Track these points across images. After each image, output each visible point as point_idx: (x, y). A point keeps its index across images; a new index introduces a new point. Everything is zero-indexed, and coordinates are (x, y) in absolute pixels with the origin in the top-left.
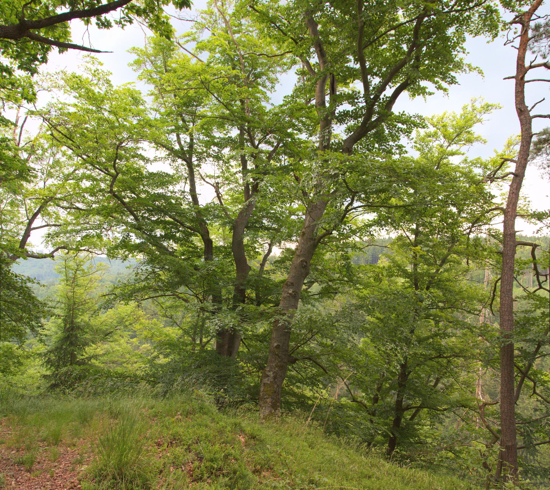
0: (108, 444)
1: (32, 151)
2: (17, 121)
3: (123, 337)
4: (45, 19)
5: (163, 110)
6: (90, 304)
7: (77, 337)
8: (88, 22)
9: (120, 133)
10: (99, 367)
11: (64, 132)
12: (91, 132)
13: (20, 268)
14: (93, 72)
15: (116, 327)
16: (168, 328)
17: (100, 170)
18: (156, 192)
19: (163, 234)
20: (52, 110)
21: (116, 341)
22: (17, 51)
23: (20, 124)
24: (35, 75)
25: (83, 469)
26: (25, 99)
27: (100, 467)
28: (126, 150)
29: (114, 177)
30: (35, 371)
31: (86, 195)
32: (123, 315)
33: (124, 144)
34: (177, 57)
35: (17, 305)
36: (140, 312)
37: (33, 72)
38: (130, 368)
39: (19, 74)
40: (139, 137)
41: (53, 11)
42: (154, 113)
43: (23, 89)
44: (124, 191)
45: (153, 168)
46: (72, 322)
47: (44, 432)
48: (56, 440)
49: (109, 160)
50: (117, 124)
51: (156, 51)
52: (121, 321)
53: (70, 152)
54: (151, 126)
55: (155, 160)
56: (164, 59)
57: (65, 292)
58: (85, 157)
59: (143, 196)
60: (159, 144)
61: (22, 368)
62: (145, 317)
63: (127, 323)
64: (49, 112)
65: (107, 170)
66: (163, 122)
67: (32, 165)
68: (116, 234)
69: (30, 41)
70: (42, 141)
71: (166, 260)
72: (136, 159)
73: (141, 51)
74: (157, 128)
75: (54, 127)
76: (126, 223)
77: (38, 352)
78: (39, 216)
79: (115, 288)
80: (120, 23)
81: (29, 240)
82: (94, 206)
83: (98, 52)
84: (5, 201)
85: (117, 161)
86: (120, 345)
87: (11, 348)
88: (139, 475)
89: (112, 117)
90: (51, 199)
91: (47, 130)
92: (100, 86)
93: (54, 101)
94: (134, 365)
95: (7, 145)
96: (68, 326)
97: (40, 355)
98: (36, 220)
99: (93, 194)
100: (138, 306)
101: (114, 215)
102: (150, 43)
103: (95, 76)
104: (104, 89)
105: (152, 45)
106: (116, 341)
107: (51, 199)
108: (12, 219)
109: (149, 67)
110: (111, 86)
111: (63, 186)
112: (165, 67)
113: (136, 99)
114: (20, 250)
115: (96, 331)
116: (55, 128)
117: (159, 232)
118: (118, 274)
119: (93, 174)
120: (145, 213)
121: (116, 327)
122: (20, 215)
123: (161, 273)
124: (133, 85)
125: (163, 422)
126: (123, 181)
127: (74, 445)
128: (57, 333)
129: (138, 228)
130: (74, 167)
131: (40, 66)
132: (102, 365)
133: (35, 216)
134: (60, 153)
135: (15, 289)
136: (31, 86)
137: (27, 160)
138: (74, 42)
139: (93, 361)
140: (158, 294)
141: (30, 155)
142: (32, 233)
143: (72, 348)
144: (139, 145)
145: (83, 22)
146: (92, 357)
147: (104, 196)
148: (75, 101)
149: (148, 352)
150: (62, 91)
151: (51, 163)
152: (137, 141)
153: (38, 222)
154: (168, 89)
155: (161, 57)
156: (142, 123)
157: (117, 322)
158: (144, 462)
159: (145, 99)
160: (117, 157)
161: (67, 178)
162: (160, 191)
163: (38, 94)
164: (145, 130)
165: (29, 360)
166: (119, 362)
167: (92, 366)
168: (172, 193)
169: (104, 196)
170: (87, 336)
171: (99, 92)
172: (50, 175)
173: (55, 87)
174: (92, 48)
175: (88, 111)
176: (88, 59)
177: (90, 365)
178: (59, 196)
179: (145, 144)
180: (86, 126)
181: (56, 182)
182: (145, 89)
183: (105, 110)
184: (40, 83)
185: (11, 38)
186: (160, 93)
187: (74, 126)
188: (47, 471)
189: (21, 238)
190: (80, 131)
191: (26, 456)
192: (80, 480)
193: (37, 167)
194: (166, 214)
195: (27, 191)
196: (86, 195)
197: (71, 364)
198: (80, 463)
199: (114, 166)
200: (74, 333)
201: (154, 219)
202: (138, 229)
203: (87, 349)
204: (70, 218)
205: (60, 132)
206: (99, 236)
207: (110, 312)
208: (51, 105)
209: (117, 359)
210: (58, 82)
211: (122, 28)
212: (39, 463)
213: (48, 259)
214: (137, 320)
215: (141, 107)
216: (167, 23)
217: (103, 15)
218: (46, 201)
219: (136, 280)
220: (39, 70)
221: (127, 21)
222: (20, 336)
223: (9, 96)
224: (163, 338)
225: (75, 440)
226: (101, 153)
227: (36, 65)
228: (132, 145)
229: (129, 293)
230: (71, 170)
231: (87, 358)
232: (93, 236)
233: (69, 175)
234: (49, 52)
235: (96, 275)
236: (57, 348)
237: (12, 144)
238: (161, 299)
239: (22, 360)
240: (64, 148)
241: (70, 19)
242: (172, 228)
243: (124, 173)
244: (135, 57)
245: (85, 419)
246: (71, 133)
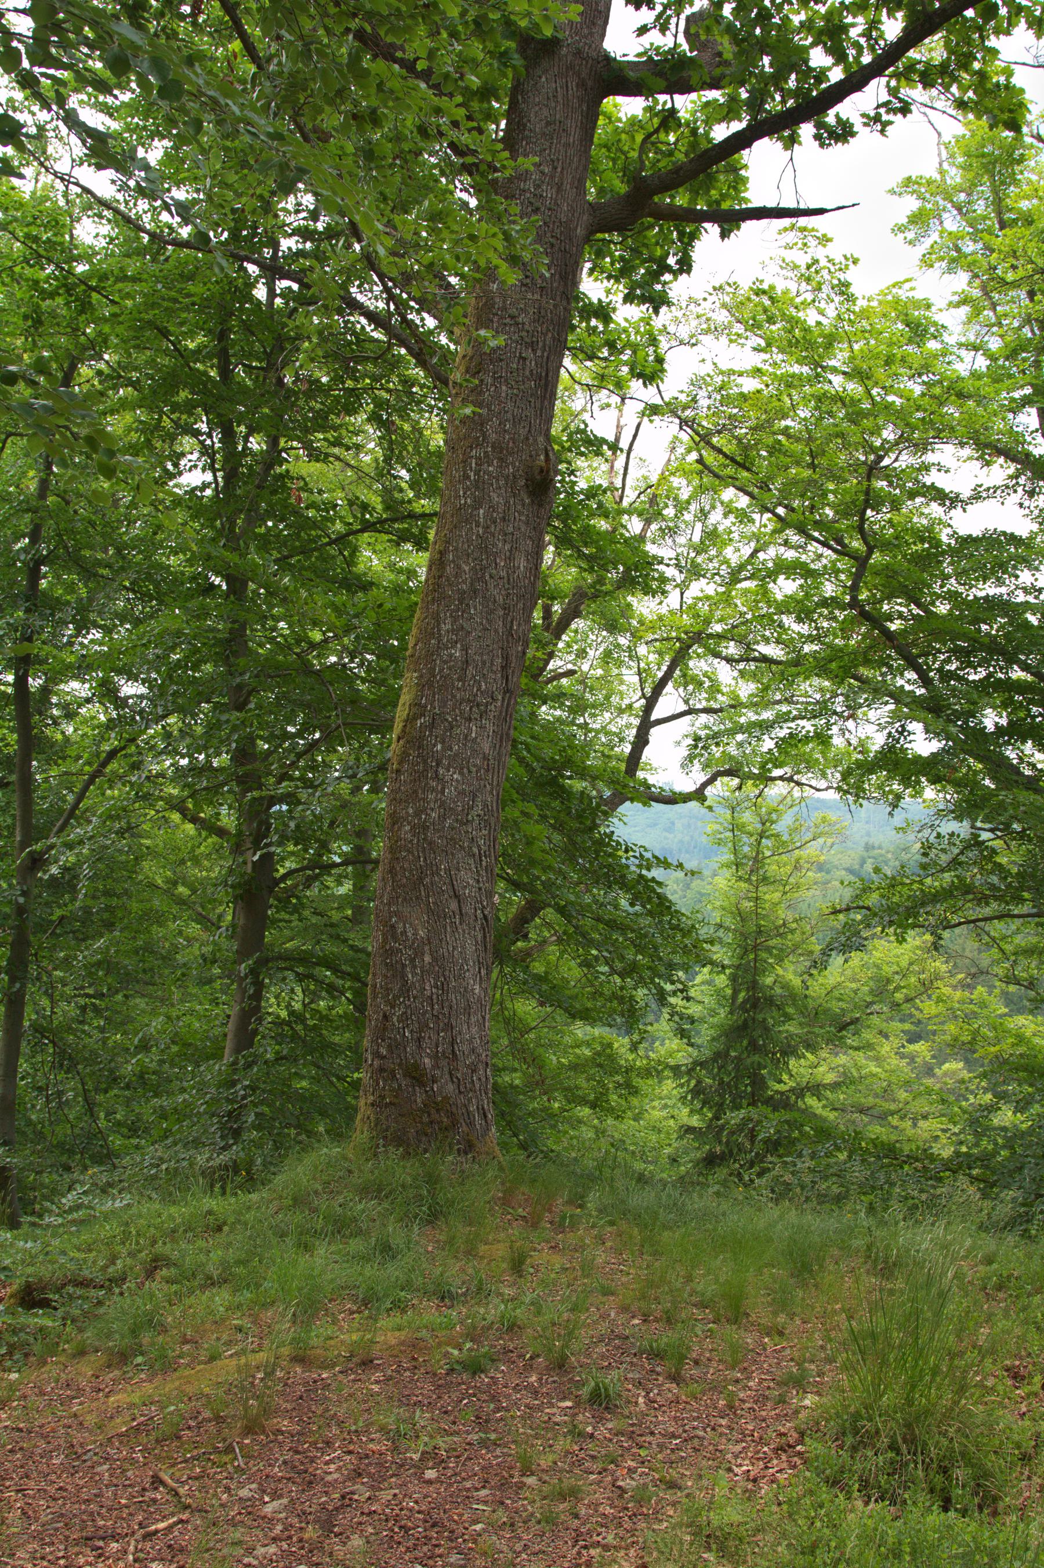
0: (867, 1345)
1: (651, 512)
2: (617, 439)
3: (886, 1037)
4: (691, 161)
5: (994, 344)
6: (797, 937)
7: (767, 1029)
8: (791, 142)
9: (876, 431)
10: (825, 1120)
11: (734, 451)
12: (798, 440)
13: (633, 826)
14: (803, 270)
15: (869, 1004)
16: (1021, 1020)
17: (825, 544)
18: (981, 594)
19: (1004, 722)
20: (703, 393)
21: (869, 1046)
22: (622, 258)
23: (624, 444)
24: (664, 309)
25: (807, 1402)
26: (640, 376)
27: (852, 1409)
28: (888, 474)
29: (861, 562)
30: (665, 1112)
31: (788, 620)
32: (887, 970)
33: (886, 462)
34: (1034, 178)
35: (623, 928)
36: (940, 965)
37: (658, 302)
38: (910, 1132)
39: (627, 314)
40: (923, 430)
41: (707, 134)
42: (967, 355)
43: (634, 352)
44: (889, 597)
45: (970, 522)
46: (754, 986)
47: (705, 1285)
48: (734, 1311)
49: (843, 512)
50: (866, 406)
51: (970, 175)
52: (882, 988)
53: (743, 501)
54: (961, 395)
55: (977, 496)
56: (995, 192)
57: (733, 899)
58: (781, 511)
59: (942, 608)
60: (989, 449)
61: (635, 1101)
62: (954, 981)
63: (899, 996)
64: (695, 400)
65: (839, 541)
66: (997, 377)
67: (651, 549)
68: (870, 729)
69: (651, 227)
70: (676, 481)
71: (1016, 805)
72: (919, 500)
73: (929, 182)
74: (981, 400)
75: (703, 439)
76: (898, 696)
77: (672, 1062)
78: (669, 687)
79: (866, 890)
80: (877, 119)
81: (648, 754)
82: (807, 648)
83: (821, 211)
84: (591, 653)
85: (869, 513)
86: (877, 1059)
87: (610, 1045)
88: (963, 1455)
89: (854, 388)
90: (698, 637)
91: (689, 451)
92: (823, 305)
93: (708, 368)
94: (921, 1123)
95: (600, 505)
96: (742, 995)
97: (676, 1070)
98: (661, 700)
99: (804, 614)
100: (936, 947)
101: (865, 672)
102: (952, 156)
103: (808, 280)
104: (831, 313)
105: (960, 160)
106: (869, 1046)
107: (698, 637)
108: (607, 698)
109: (952, 222)
110: (851, 299)
111: (726, 599)
112: (999, 213)
113: (918, 325)
114: (628, 783)
115: (815, 1015)
116: (709, 443)
117: (991, 719)
118: (868, 847)
119: (804, 558)
120: (948, 661)
121: (869, 1004)
122: (624, 688)
123: (998, 844)
124: (907, 286)
125: (1024, 1309)
126: (888, 573)
127: (781, 1334)
128: (713, 1013)
129: (933, 709)
130: (753, 544)
131: (674, 285)
132: (832, 1116)
133: (659, 688)
134: (720, 510)
135: (623, 884)
136: (653, 341)
137: (641, 538)
138: (756, 203)
139: (811, 1101)
140: (987, 911)
141: (648, 522)
142: (655, 732)
143: (756, 1058)
144: (930, 458)
145: (779, 145)
146: (808, 1088)
147: (834, 619)
148: (757, 360)
149: (961, 1089)
150: (724, 339)
151: (697, 538)
152: (923, 447)
153: (670, 702)
154: (1010, 277)
155: (985, 189)
156: (937, 391)
157: (871, 991)
158: (978, 1421)
159: (941, 318)
160: (871, 500)
161: (735, 576)
162: (989, 589)
163: (668, 357)
164: (950, 412)
165: (650, 1082)
166: (875, 1112)
167: (806, 1111)
168: (1026, 591)
169: (834, 619)
170: (792, 1028)
171: (819, 323)
172: (695, 572)
173: (707, 332)
174: (802, 206)
175: (790, 382)
176: (791, 237)
177: (803, 1111)
178: (718, 628)
179: (945, 453)
180: (783, 423)
181: (710, 589)
182: (941, 290)
183: (835, 370)
184: (671, 329)
185: (609, 231)
186: (986, 294)
187: (754, 429)
188: (716, 1388)
189: (627, 749)
190: (770, 441)
191: (666, 1338)
192: (802, 1434)
193: (665, 552)
194: (1011, 660)
195: (641, 623)
196: (788, 620)
197: (753, 1104)
198: (799, 1383)
199: (861, 529)
200: (760, 1017)
201: (977, 677)
202: (930, 710)
203: (792, 1062)
204: (746, 690)
205: (720, 451)
206: (822, 738)
207: (856, 958)
208: (699, 382)
209: (871, 1101)
210: (714, 316)
211: (882, 132)
212: (696, 1362)
213: (694, 804)
214: (926, 987)
215: (932, 345)
216: (1007, 87)
217: (832, 112)
218: (687, 642)
219: (924, 867)
220: (671, 294)
221: (895, 111)
222: (631, 1017)
223: (602, 377)
224: (1006, 1045)
225: (782, 1319)
226: (824, 495)
227: (665, 283)
228: (912, 460)
229: (900, 903)
230: (747, 551)
231: (792, 1090)
232: (807, 739)
233: (741, 567)
234: (697, 244)
235: (812, 850)
236: (717, 1055)
237: (608, 499)
238: (997, 928)
239: (637, 1082)
240: (729, 494)
241: (749, 145)
242: (1031, 702)
243: (886, 546)
244: (911, 204)
245: (804, 1264)
246: (746, 449)
